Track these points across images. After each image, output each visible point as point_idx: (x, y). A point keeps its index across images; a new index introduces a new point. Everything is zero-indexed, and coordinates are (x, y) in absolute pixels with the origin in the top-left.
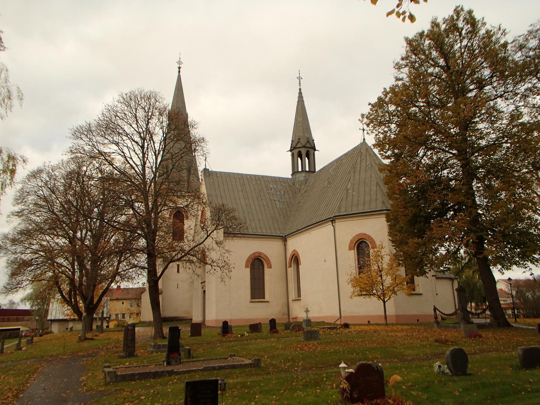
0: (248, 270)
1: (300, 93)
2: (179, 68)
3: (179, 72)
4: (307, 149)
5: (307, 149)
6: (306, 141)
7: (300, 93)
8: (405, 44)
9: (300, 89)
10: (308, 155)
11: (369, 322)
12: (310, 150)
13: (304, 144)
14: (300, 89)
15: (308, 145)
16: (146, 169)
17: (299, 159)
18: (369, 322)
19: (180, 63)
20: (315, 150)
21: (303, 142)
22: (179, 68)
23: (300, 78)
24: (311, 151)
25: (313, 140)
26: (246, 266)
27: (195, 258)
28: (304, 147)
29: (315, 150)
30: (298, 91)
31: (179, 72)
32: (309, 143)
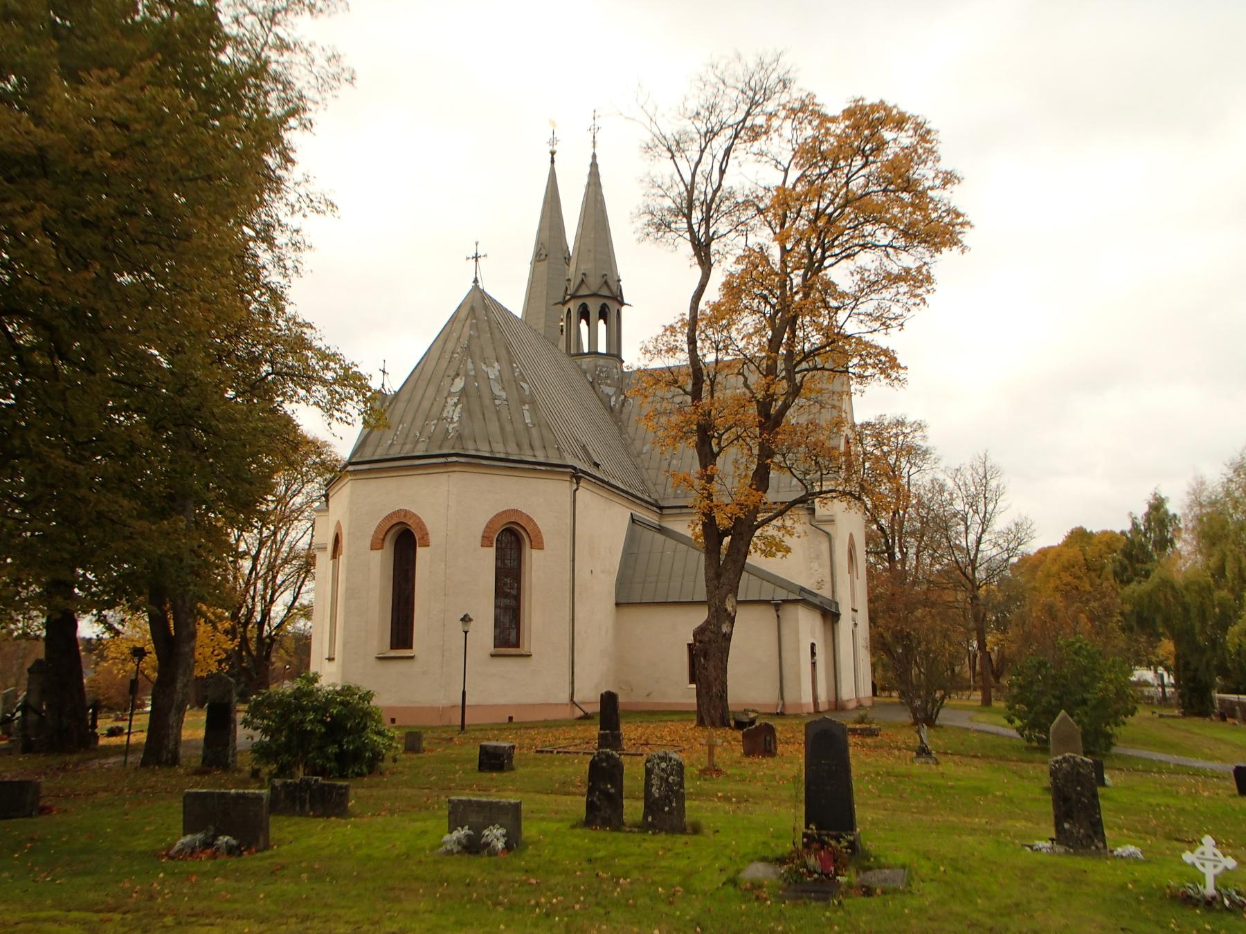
0: (492, 552)
1: (594, 165)
2: (553, 153)
3: (553, 161)
4: (602, 301)
5: (580, 302)
6: (600, 281)
7: (594, 165)
8: (1141, 510)
9: (594, 156)
10: (603, 315)
11: (511, 718)
12: (608, 302)
13: (594, 289)
14: (594, 156)
15: (605, 292)
16: (685, 347)
17: (583, 322)
18: (511, 718)
19: (553, 141)
20: (622, 303)
21: (594, 283)
22: (553, 153)
23: (594, 130)
24: (613, 306)
25: (619, 281)
26: (486, 541)
27: (724, 437)
28: (594, 295)
29: (622, 303)
30: (590, 160)
31: (553, 161)
32: (608, 286)
